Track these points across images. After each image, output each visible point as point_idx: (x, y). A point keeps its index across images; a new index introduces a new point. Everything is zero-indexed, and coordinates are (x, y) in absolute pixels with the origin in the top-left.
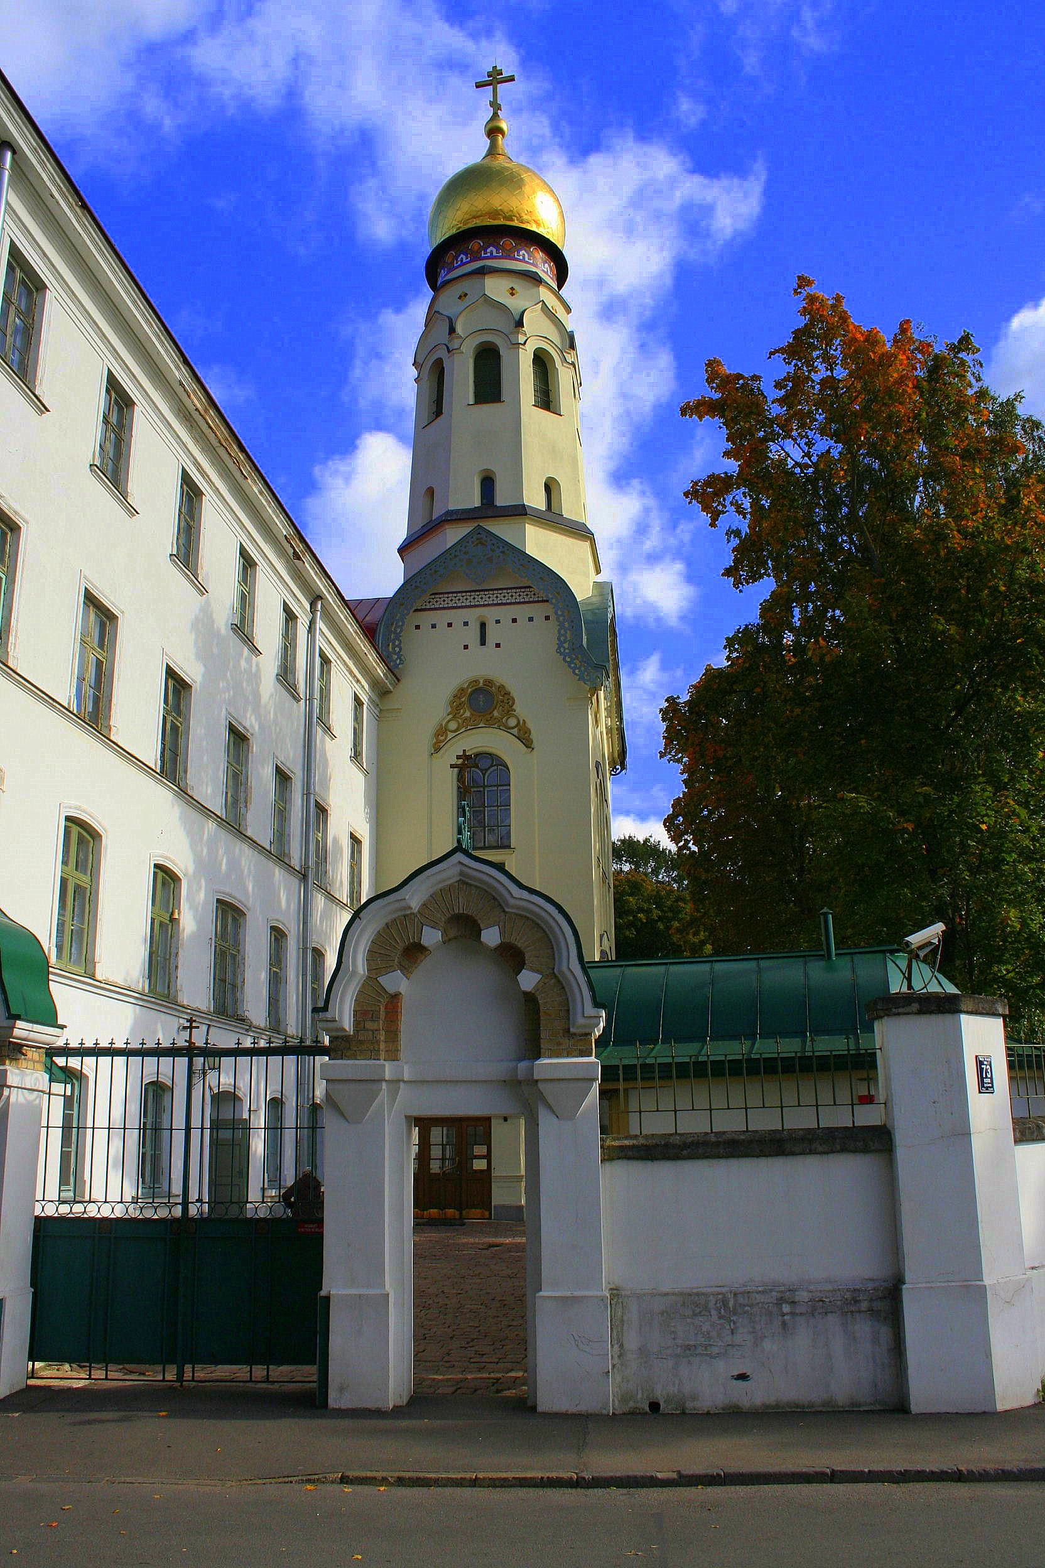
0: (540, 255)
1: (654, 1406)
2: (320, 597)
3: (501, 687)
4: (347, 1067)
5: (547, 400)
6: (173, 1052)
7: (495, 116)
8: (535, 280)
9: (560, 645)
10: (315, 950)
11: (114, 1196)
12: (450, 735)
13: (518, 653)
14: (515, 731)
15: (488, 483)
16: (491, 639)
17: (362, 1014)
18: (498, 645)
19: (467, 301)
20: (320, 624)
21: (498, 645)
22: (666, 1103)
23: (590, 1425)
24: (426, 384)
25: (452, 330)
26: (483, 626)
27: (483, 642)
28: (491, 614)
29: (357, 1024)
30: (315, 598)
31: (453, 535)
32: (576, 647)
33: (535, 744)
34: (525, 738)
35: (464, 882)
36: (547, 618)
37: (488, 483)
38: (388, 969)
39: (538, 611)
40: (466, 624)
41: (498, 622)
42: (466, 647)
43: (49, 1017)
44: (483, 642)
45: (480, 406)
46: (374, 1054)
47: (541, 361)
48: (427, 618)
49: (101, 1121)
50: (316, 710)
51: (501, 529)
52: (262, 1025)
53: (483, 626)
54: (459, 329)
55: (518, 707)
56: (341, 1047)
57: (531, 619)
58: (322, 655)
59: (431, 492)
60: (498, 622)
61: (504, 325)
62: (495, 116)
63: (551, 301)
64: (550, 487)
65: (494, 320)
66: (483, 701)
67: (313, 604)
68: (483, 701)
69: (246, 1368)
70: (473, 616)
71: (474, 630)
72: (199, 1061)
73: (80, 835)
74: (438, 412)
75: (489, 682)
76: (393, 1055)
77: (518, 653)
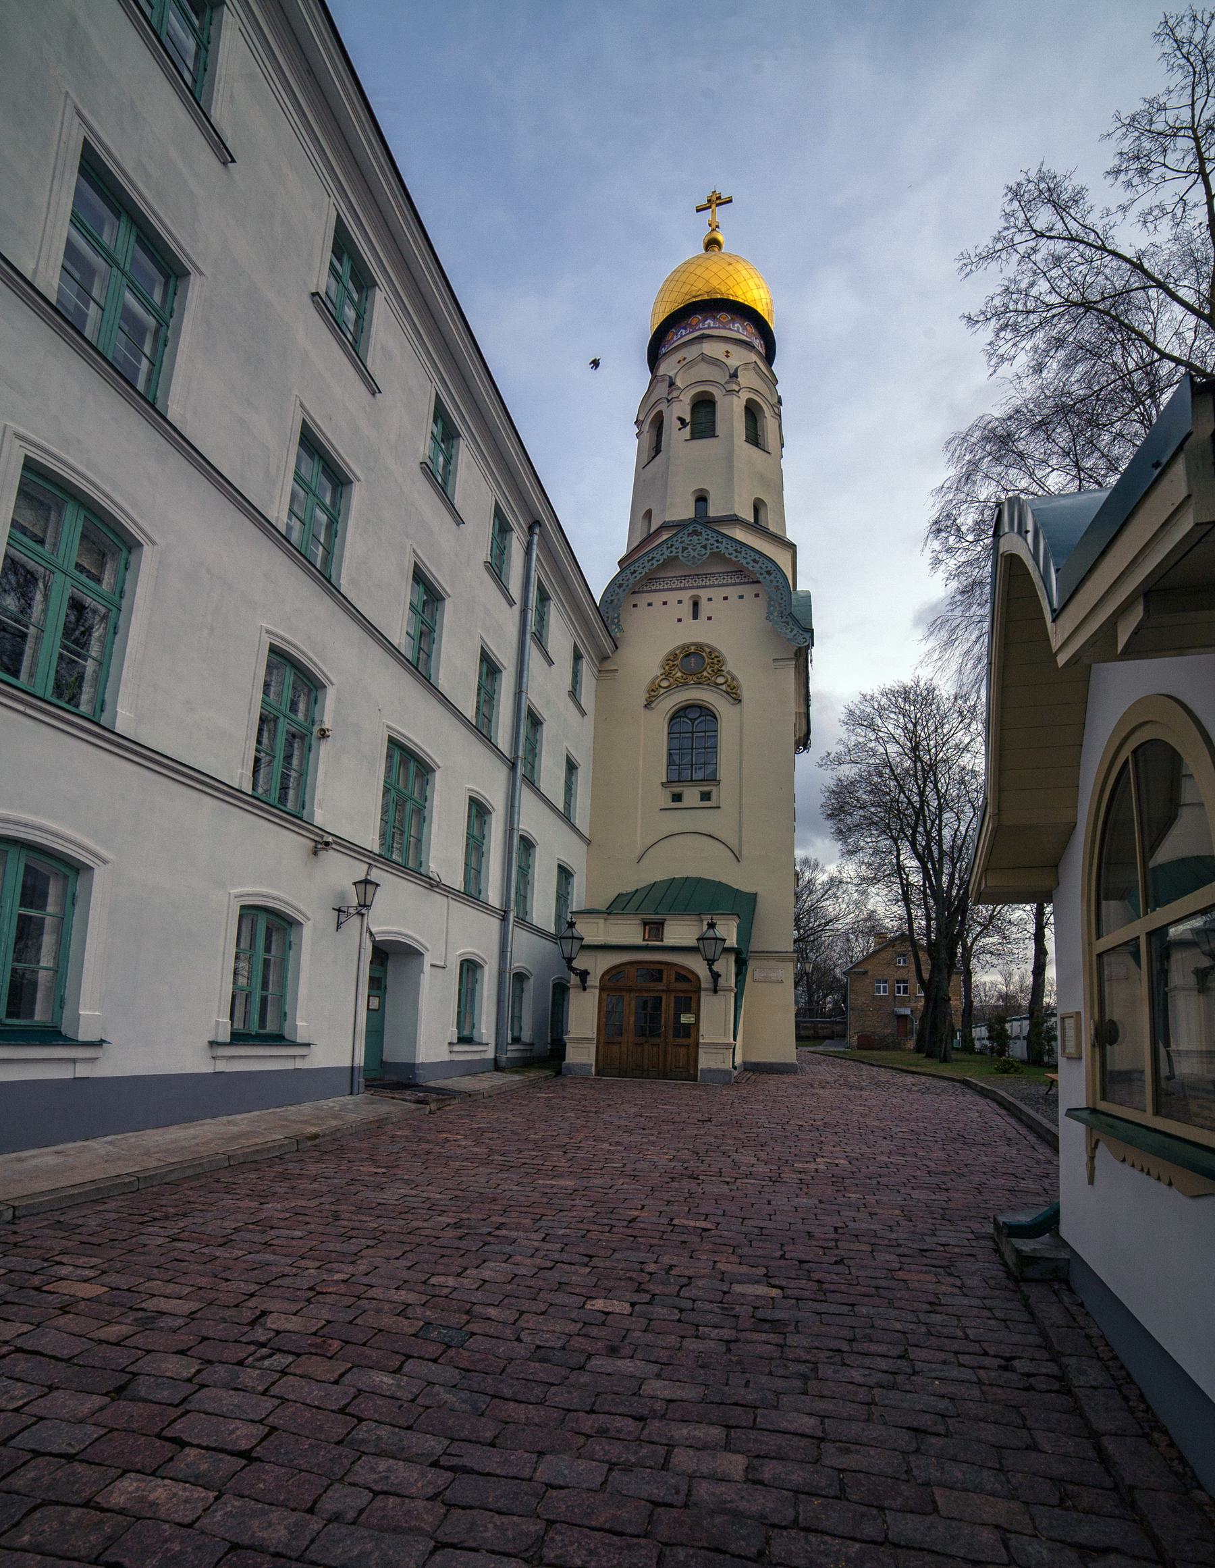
3: (713, 650)
5: (755, 437)
10: (523, 839)
12: (662, 691)
14: (723, 687)
15: (701, 499)
18: (710, 618)
21: (710, 618)
23: (1065, 196)
26: (696, 604)
27: (695, 617)
28: (704, 594)
30: (534, 524)
34: (734, 695)
36: (757, 596)
37: (701, 499)
40: (680, 602)
41: (710, 600)
42: (679, 620)
44: (695, 617)
47: (752, 412)
50: (531, 628)
52: (737, 1478)
53: (696, 604)
54: (678, 383)
57: (741, 597)
60: (710, 600)
61: (722, 378)
65: (704, 371)
66: (694, 662)
67: (531, 528)
68: (694, 662)
70: (686, 596)
71: (687, 606)
73: (101, 236)
74: (657, 450)
75: (700, 647)
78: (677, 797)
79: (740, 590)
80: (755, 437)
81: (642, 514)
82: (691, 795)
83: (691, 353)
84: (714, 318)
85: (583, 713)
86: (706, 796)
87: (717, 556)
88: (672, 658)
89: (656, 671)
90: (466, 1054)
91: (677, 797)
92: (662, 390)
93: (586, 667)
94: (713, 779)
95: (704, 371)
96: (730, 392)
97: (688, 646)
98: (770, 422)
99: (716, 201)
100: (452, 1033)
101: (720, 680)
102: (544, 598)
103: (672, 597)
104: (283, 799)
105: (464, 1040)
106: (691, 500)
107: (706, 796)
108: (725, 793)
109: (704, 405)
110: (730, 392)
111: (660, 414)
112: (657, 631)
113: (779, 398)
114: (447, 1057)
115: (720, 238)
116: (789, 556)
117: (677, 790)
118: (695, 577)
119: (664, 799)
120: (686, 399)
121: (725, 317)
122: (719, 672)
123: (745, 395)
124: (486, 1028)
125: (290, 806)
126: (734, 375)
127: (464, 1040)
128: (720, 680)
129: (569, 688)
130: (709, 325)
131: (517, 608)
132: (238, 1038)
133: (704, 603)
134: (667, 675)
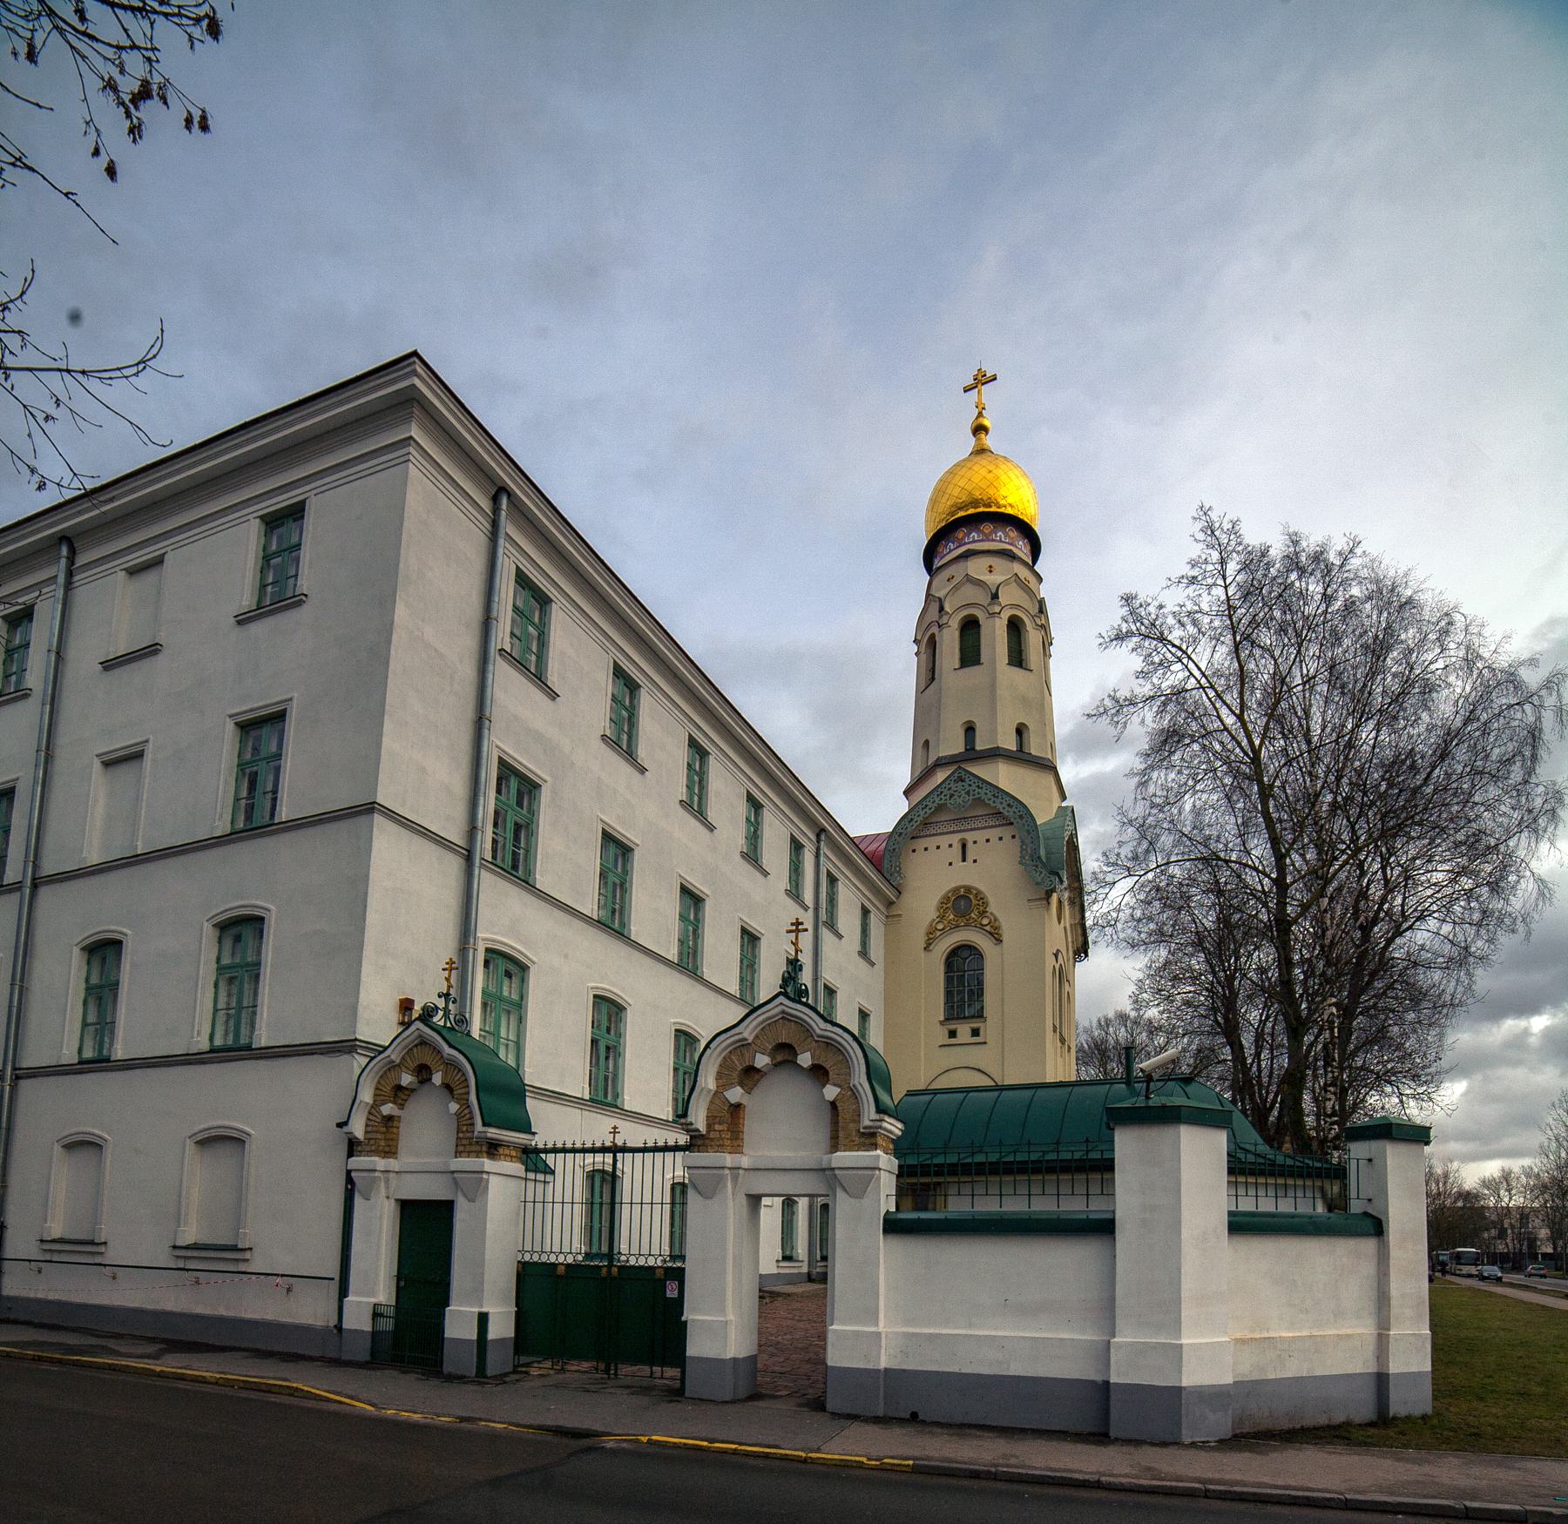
0: (1014, 534)
1: (914, 1416)
2: (823, 830)
3: (979, 892)
4: (698, 1158)
5: (1017, 658)
6: (603, 1150)
7: (980, 415)
8: (1010, 556)
9: (1022, 857)
11: (655, 1251)
13: (991, 866)
15: (970, 729)
16: (970, 856)
17: (711, 1120)
19: (955, 582)
20: (824, 849)
22: (966, 1189)
24: (924, 657)
25: (941, 609)
26: (964, 846)
27: (964, 860)
28: (970, 837)
29: (709, 1126)
30: (820, 832)
31: (941, 776)
32: (1035, 858)
33: (1005, 938)
35: (786, 1017)
37: (970, 729)
38: (731, 1085)
39: (1006, 832)
43: (525, 1127)
44: (964, 860)
45: (966, 670)
46: (720, 1148)
47: (1015, 626)
48: (931, 842)
49: (626, 1199)
51: (981, 770)
53: (964, 846)
54: (947, 608)
55: (992, 908)
56: (696, 1142)
58: (829, 874)
59: (927, 743)
61: (984, 599)
62: (980, 415)
63: (1024, 573)
64: (1020, 731)
65: (970, 594)
68: (964, 905)
69: (647, 1368)
70: (955, 839)
71: (957, 847)
72: (619, 1155)
75: (968, 889)
76: (737, 1149)
77: (991, 866)
78: (953, 1034)
79: (997, 832)
80: (1017, 658)
81: (923, 745)
82: (964, 1030)
83: (957, 571)
84: (979, 532)
85: (873, 964)
86: (975, 1032)
87: (979, 802)
88: (946, 899)
89: (932, 914)
90: (788, 1269)
91: (953, 1034)
92: (933, 614)
93: (875, 920)
94: (980, 1015)
95: (970, 594)
96: (993, 615)
97: (957, 889)
98: (1033, 637)
99: (982, 380)
100: (778, 1253)
101: (985, 921)
102: (832, 880)
103: (943, 841)
104: (515, 867)
105: (787, 1258)
106: (961, 733)
107: (975, 1032)
108: (990, 1028)
109: (970, 627)
110: (993, 615)
111: (933, 636)
112: (933, 874)
113: (1041, 603)
114: (775, 1271)
115: (986, 422)
116: (1051, 779)
117: (952, 1027)
118: (962, 821)
119: (941, 1035)
120: (955, 623)
121: (987, 527)
122: (983, 914)
123: (1006, 615)
124: (801, 1250)
125: (520, 873)
126: (995, 596)
127: (787, 1258)
128: (985, 921)
129: (858, 948)
130: (974, 540)
131: (811, 911)
132: (947, 1019)
133: (970, 845)
134: (942, 917)
